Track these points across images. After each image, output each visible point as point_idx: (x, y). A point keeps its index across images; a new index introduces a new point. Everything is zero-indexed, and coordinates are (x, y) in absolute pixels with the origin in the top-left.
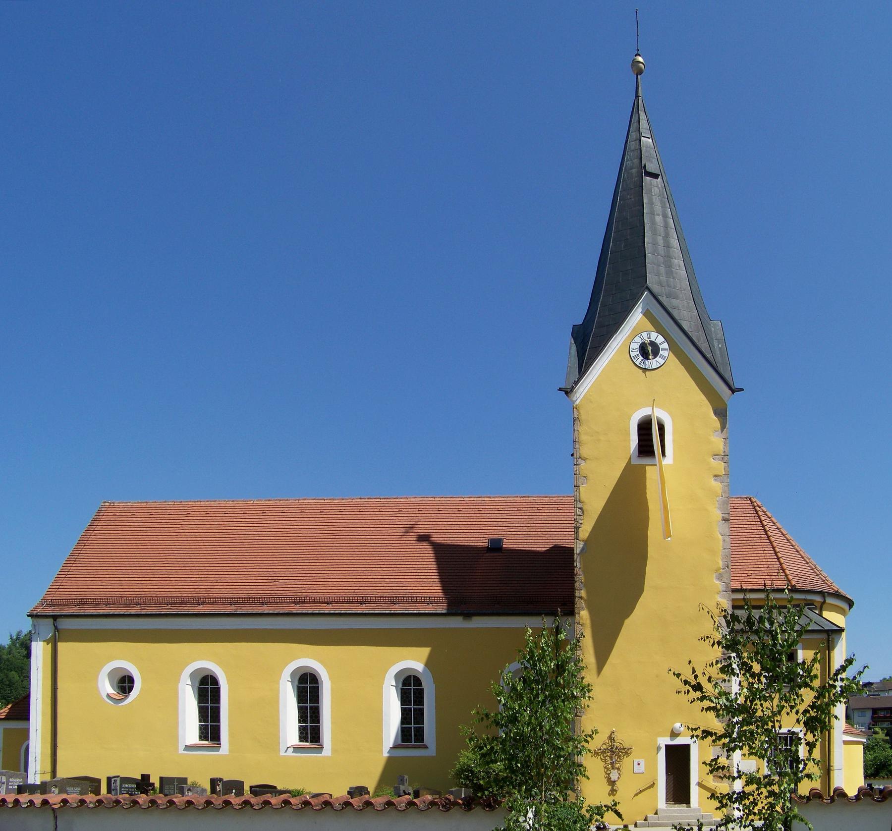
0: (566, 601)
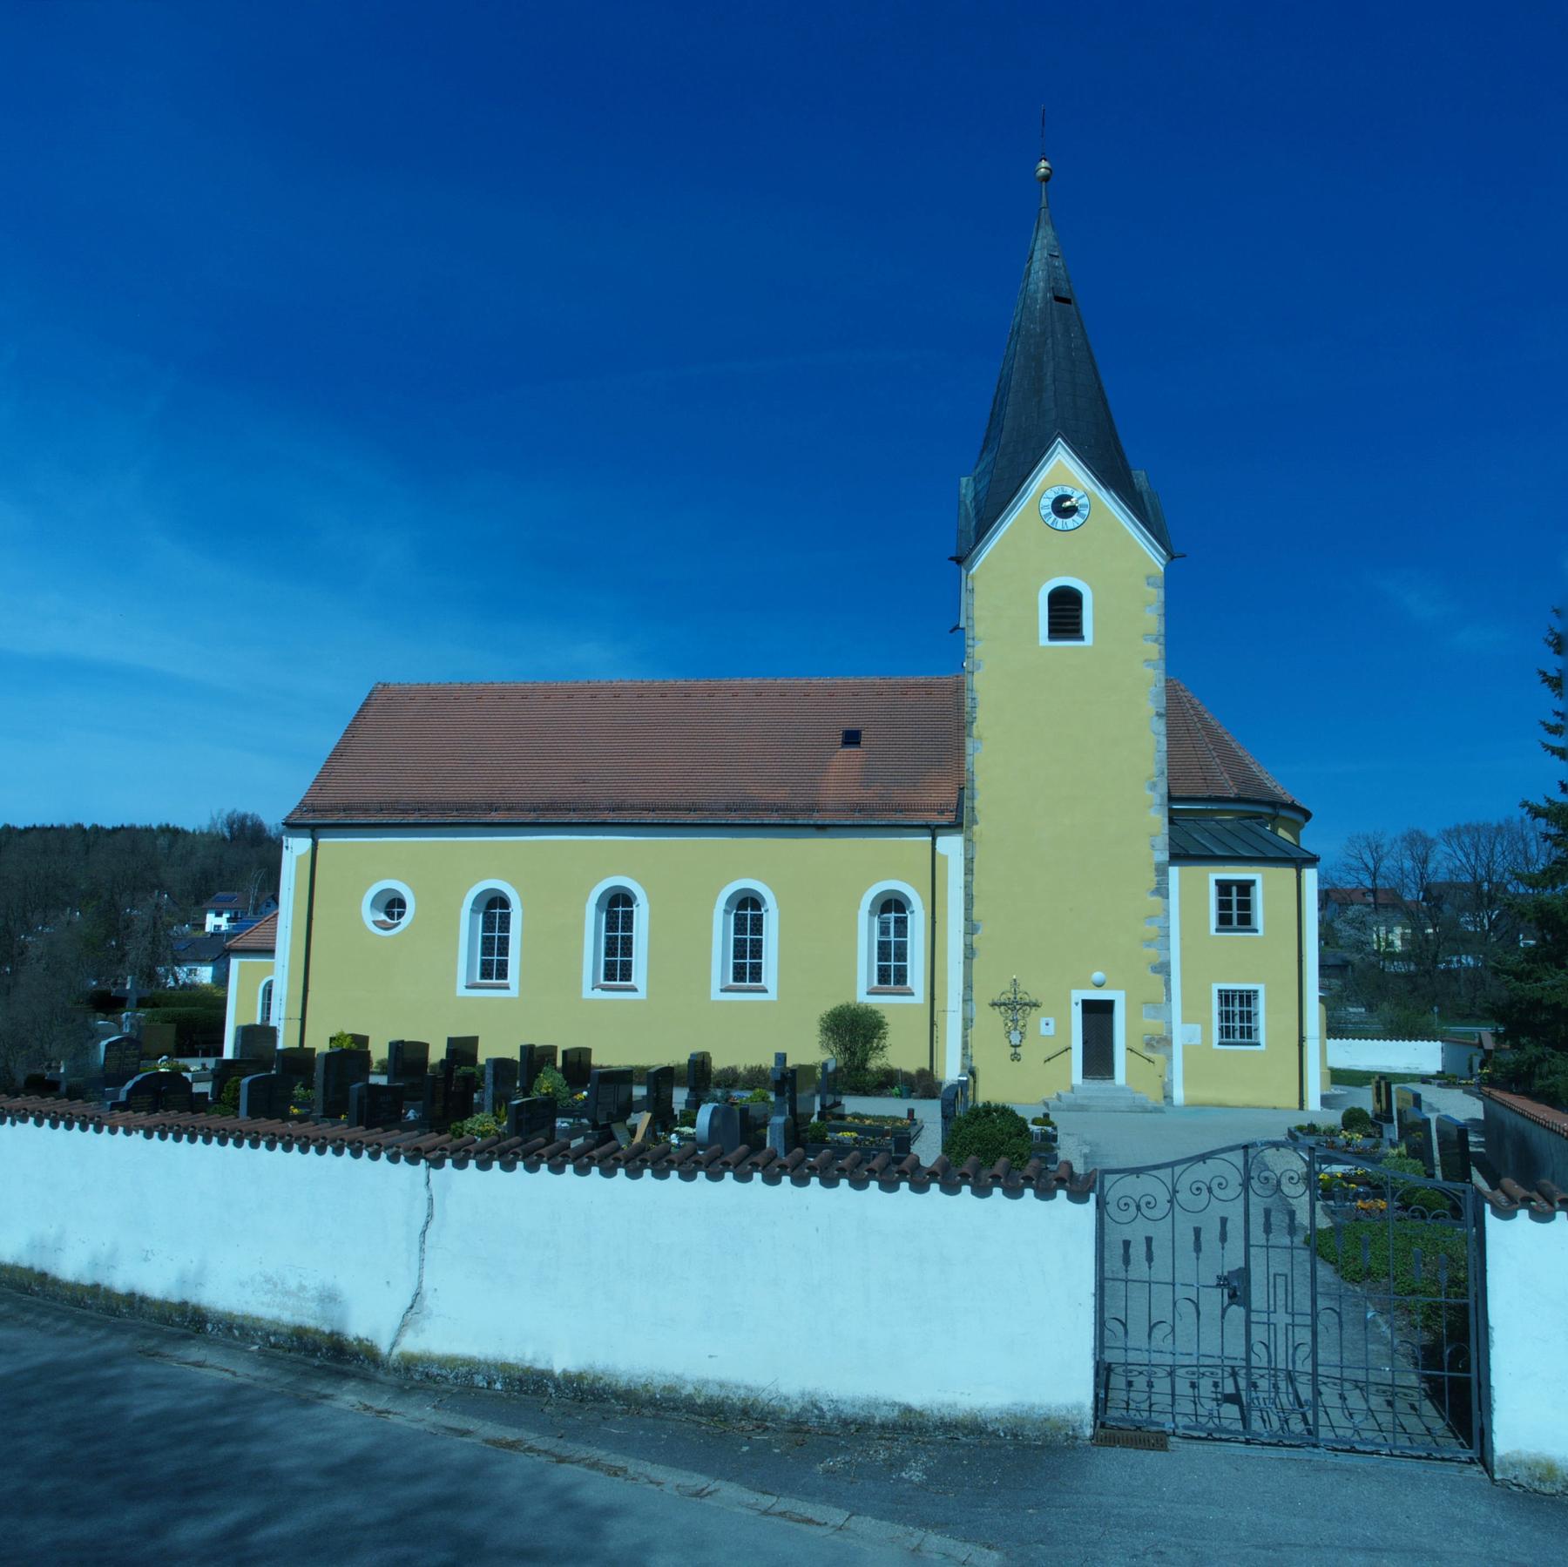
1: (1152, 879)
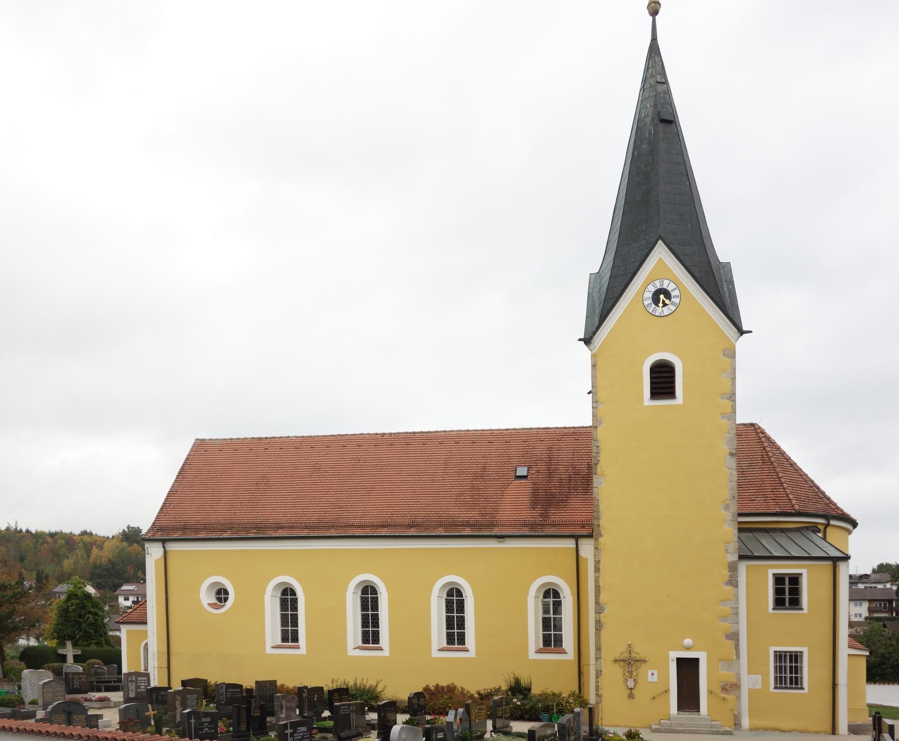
0: (585, 524)
1: (726, 573)
